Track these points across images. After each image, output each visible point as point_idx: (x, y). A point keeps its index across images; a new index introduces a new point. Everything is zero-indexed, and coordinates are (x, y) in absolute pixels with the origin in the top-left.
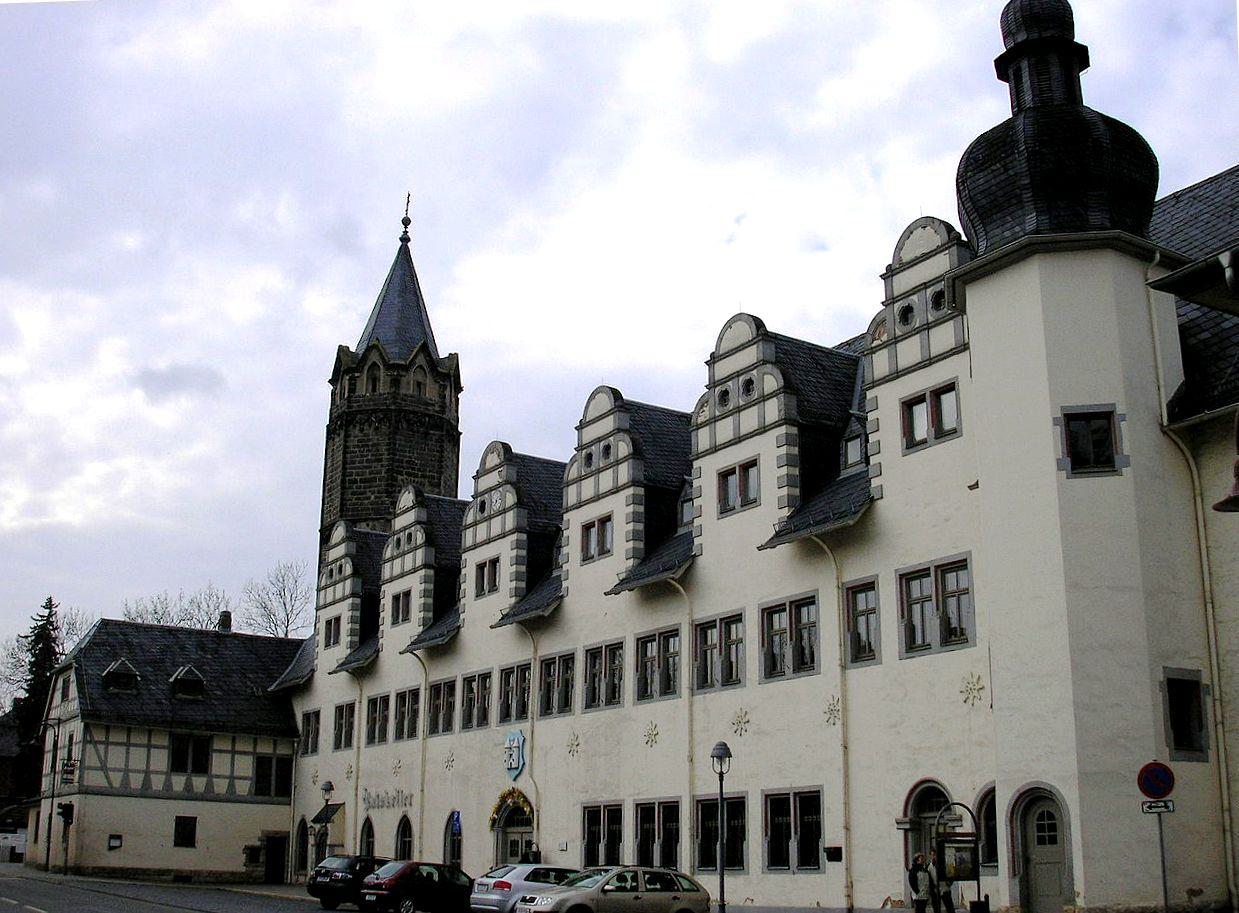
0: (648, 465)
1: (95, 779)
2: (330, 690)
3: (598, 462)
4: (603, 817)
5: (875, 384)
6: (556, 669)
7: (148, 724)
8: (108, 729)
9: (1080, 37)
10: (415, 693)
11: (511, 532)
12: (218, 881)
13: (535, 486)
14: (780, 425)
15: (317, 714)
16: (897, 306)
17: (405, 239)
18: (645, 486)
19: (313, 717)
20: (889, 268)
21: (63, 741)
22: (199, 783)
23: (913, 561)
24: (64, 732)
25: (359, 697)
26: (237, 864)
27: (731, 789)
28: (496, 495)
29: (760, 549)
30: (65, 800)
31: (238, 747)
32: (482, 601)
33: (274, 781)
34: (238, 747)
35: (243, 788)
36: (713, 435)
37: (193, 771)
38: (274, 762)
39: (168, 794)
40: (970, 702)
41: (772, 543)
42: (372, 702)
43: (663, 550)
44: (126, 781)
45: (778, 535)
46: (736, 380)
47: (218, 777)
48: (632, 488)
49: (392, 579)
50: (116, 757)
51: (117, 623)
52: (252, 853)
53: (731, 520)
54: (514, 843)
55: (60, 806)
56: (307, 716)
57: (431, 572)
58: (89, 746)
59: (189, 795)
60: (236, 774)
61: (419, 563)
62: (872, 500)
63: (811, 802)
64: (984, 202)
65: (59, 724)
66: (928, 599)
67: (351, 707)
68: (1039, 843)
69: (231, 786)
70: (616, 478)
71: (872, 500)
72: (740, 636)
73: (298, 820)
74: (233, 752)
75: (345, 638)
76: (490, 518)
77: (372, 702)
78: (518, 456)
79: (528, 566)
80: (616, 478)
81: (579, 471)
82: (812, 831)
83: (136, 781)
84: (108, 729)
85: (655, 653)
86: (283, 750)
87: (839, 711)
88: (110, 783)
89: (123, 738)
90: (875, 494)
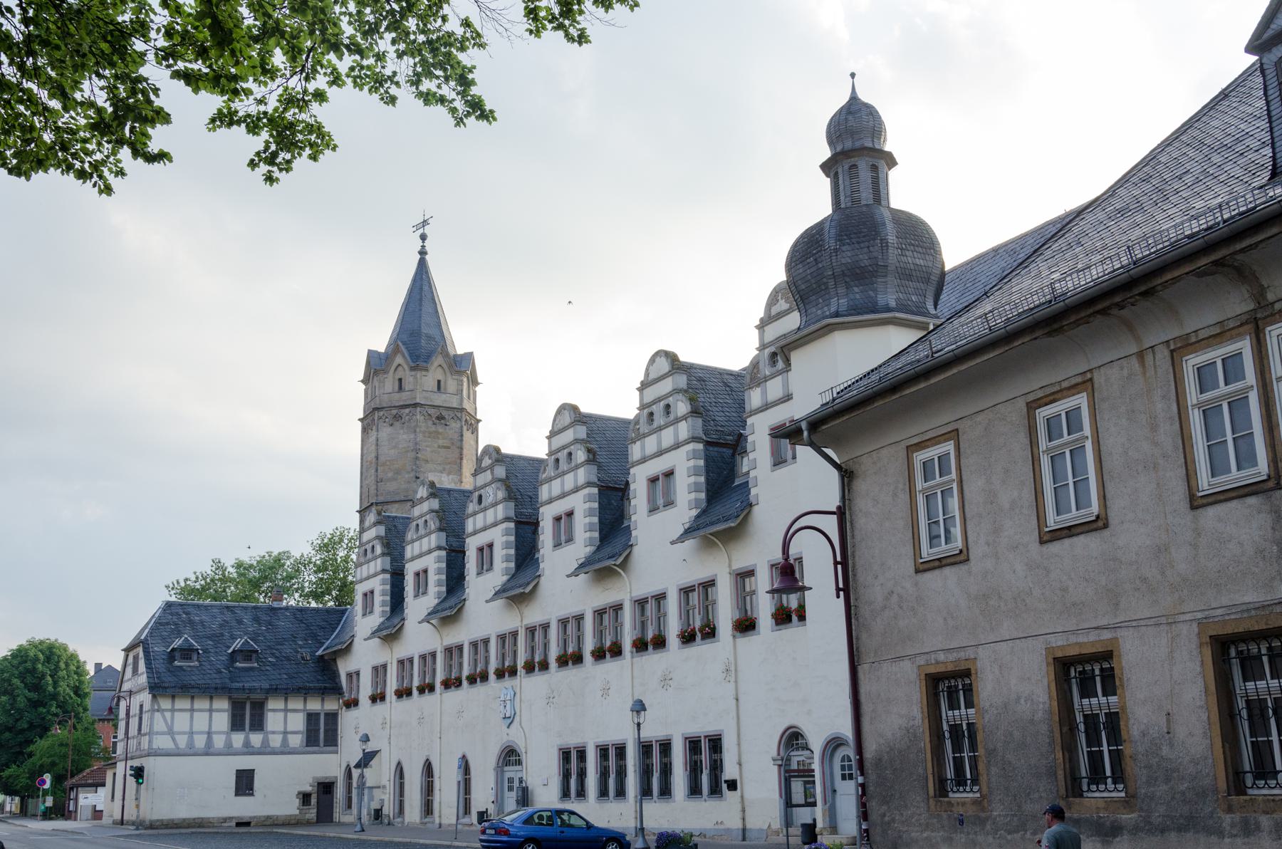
0: (600, 468)
1: (163, 742)
2: (364, 656)
3: (660, 420)
4: (705, 746)
7: (211, 692)
8: (173, 697)
9: (826, 183)
10: (433, 655)
11: (687, 442)
12: (271, 824)
13: (520, 481)
15: (358, 673)
17: (423, 253)
18: (598, 486)
19: (354, 676)
20: (762, 320)
21: (135, 710)
22: (256, 739)
24: (136, 701)
25: (390, 656)
26: (289, 807)
27: (652, 732)
28: (490, 490)
30: (136, 763)
32: (481, 578)
33: (322, 733)
35: (296, 741)
38: (322, 717)
39: (229, 751)
41: (682, 539)
42: (401, 662)
43: (725, 497)
44: (191, 744)
45: (582, 566)
47: (273, 733)
49: (475, 533)
50: (181, 721)
52: (305, 798)
54: (511, 780)
56: (349, 675)
58: (157, 715)
59: (248, 750)
61: (379, 568)
62: (751, 505)
63: (716, 743)
64: (803, 287)
67: (385, 666)
69: (285, 741)
70: (676, 434)
71: (751, 505)
74: (286, 710)
75: (378, 608)
76: (485, 509)
78: (507, 456)
80: (676, 434)
82: (717, 767)
83: (200, 742)
85: (696, 602)
87: (731, 671)
88: (176, 744)
90: (752, 499)
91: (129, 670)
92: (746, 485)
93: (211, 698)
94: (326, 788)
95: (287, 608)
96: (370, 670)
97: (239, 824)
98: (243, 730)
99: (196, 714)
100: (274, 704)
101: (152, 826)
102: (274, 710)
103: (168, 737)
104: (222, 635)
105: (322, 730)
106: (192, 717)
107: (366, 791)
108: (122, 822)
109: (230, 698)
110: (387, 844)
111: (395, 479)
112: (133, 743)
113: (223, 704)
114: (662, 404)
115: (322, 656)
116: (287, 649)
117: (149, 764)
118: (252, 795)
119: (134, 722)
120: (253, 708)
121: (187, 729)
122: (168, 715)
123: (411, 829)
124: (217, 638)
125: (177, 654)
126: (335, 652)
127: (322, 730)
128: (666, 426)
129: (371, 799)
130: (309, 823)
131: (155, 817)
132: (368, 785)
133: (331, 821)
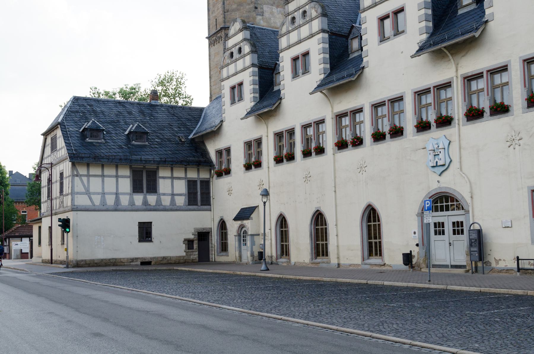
1: (82, 201)
5: (365, 10)
6: (286, 136)
7: (116, 162)
8: (88, 165)
11: (317, 33)
14: (319, 33)
16: (290, 17)
21: (56, 177)
22: (152, 199)
23: (378, 98)
26: (178, 250)
30: (63, 216)
31: (176, 175)
33: (199, 196)
34: (176, 175)
35: (181, 201)
36: (288, 39)
37: (147, 192)
39: (132, 208)
40: (361, 172)
42: (279, 136)
44: (103, 202)
45: (319, 86)
46: (298, 11)
47: (164, 194)
48: (321, 34)
50: (95, 184)
51: (86, 99)
52: (189, 243)
53: (386, 45)
55: (60, 220)
56: (219, 153)
57: (326, 35)
58: (77, 179)
59: (146, 207)
60: (175, 192)
66: (385, 116)
67: (259, 142)
68: (462, 222)
69: (173, 201)
72: (324, 130)
73: (217, 220)
77: (279, 136)
79: (433, 10)
81: (287, 27)
83: (110, 201)
84: (88, 165)
86: (204, 175)
89: (112, 172)
91: (48, 149)
92: (279, 91)
93: (117, 167)
94: (203, 236)
95: (162, 105)
96: (242, 145)
98: (142, 192)
99: (106, 179)
100: (163, 173)
101: (78, 264)
103: (86, 196)
104: (118, 121)
105: (199, 193)
106: (117, 181)
107: (248, 238)
108: (51, 262)
109: (131, 168)
111: (238, 10)
112: (56, 203)
113: (126, 172)
114: (301, 11)
115: (193, 139)
116: (167, 134)
117: (70, 215)
118: (151, 241)
119: (56, 188)
120: (148, 176)
122: (85, 179)
123: (300, 268)
124: (115, 123)
125: (88, 133)
126: (202, 136)
127: (199, 193)
128: (304, 24)
129: (253, 243)
130: (192, 263)
131: (80, 258)
132: (249, 233)
133: (209, 260)
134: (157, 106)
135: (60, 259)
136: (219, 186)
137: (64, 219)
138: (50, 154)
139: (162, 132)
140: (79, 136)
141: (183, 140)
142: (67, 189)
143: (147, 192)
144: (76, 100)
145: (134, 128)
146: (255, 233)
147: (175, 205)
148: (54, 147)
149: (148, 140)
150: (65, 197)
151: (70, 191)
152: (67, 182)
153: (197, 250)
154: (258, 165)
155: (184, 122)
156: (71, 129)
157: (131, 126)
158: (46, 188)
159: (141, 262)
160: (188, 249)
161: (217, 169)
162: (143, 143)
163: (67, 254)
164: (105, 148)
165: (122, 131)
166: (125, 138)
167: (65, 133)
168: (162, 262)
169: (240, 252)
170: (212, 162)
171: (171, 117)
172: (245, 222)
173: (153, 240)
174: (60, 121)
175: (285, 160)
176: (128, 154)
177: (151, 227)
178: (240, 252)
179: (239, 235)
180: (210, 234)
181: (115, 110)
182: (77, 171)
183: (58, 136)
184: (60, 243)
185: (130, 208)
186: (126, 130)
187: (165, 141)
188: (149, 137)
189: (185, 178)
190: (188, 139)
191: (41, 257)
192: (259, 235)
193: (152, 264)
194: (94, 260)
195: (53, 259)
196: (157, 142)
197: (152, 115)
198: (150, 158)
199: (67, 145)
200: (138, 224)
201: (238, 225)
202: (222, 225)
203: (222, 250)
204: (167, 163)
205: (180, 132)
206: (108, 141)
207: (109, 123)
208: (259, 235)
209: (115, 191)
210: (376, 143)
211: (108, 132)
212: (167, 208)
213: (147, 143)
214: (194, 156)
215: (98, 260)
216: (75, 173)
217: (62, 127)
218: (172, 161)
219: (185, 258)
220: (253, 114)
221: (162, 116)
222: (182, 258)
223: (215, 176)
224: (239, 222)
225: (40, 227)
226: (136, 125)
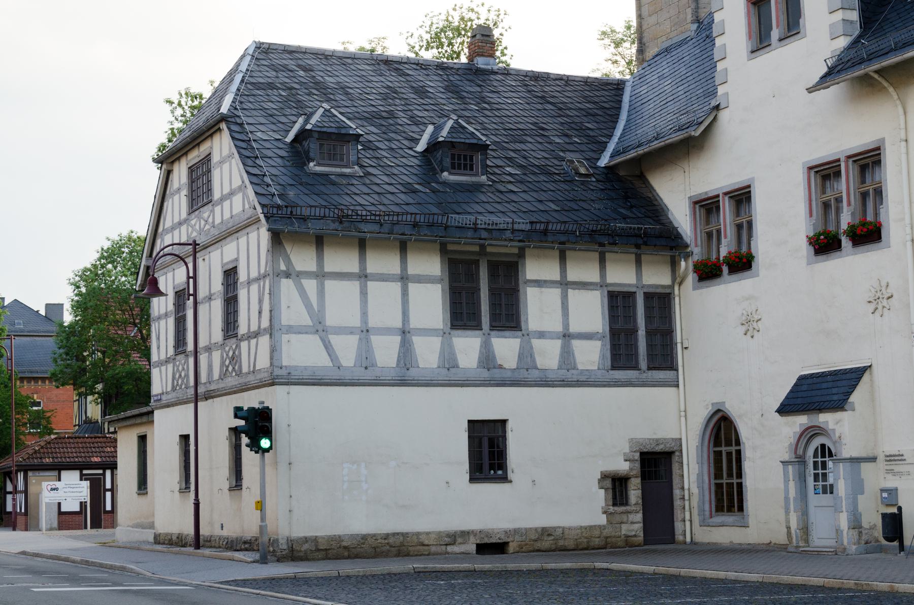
1: (303, 352)
6: (726, 207)
7: (402, 235)
12: (549, 542)
15: (742, 197)
21: (211, 280)
22: (506, 348)
26: (587, 510)
29: (810, 90)
30: (251, 400)
32: (767, 58)
33: (642, 341)
35: (591, 355)
37: (493, 327)
39: (450, 377)
44: (366, 358)
47: (541, 335)
50: (341, 302)
52: (616, 485)
55: (238, 412)
56: (707, 207)
58: (287, 285)
59: (492, 376)
60: (574, 328)
65: (195, 252)
69: (567, 355)
83: (386, 352)
86: (656, 276)
91: (178, 205)
94: (656, 464)
97: (485, 548)
98: (478, 327)
100: (539, 268)
101: (294, 552)
102: (539, 283)
104: (392, 115)
106: (405, 293)
108: (198, 542)
109: (444, 250)
110: (776, 587)
112: (212, 365)
113: (428, 264)
115: (609, 169)
116: (536, 153)
117: (276, 399)
118: (504, 479)
121: (355, 321)
122: (310, 285)
125: (313, 146)
129: (857, 487)
130: (627, 547)
131: (299, 532)
132: (848, 451)
134: (493, 72)
135: (225, 533)
136: (706, 313)
137: (252, 410)
138: (184, 215)
139: (518, 146)
140: (283, 153)
141: (582, 171)
142: (248, 316)
143: (493, 327)
144: (263, 52)
145: (445, 132)
146: (864, 455)
147: (575, 368)
148: (200, 194)
149: (485, 169)
150: (244, 345)
151: (265, 323)
152: (249, 301)
153: (640, 508)
154: (868, 234)
155: (577, 120)
156: (259, 134)
157: (430, 128)
158: (171, 321)
159: (478, 545)
160: (614, 505)
161: (696, 258)
162: (474, 179)
163: (263, 519)
164: (366, 190)
165: (406, 142)
166: (417, 162)
167: (243, 145)
168: (538, 545)
169: (804, 513)
170: (678, 236)
171: (539, 107)
172: (826, 419)
173: (510, 475)
174: (224, 109)
175: (845, 242)
176: (435, 210)
177: (504, 437)
178: (804, 513)
179: (800, 460)
180: (675, 458)
181: (378, 83)
182: (288, 262)
183: (215, 158)
184: (226, 485)
185: (443, 374)
186: (416, 141)
187: (534, 174)
188: (488, 163)
189: (602, 285)
190: (597, 168)
191: (151, 526)
192: (873, 459)
193: (512, 548)
194: (338, 539)
195: (202, 532)
196: (510, 174)
197: (483, 99)
198: (500, 220)
199: (255, 180)
200: (465, 425)
201: (798, 430)
202: (722, 431)
203: (719, 509)
204: (550, 238)
205: (571, 147)
206: (370, 170)
207: (366, 119)
208: (873, 459)
209: (399, 325)
210: (820, 257)
211: (368, 146)
212: (551, 376)
213: (484, 178)
214: (625, 218)
215: (352, 536)
216: (283, 267)
217: (234, 128)
218: (565, 233)
219: (606, 533)
220: (843, 76)
221: (512, 103)
222: (597, 533)
223: (691, 278)
224: (801, 421)
225: (143, 439)
226: (450, 123)
